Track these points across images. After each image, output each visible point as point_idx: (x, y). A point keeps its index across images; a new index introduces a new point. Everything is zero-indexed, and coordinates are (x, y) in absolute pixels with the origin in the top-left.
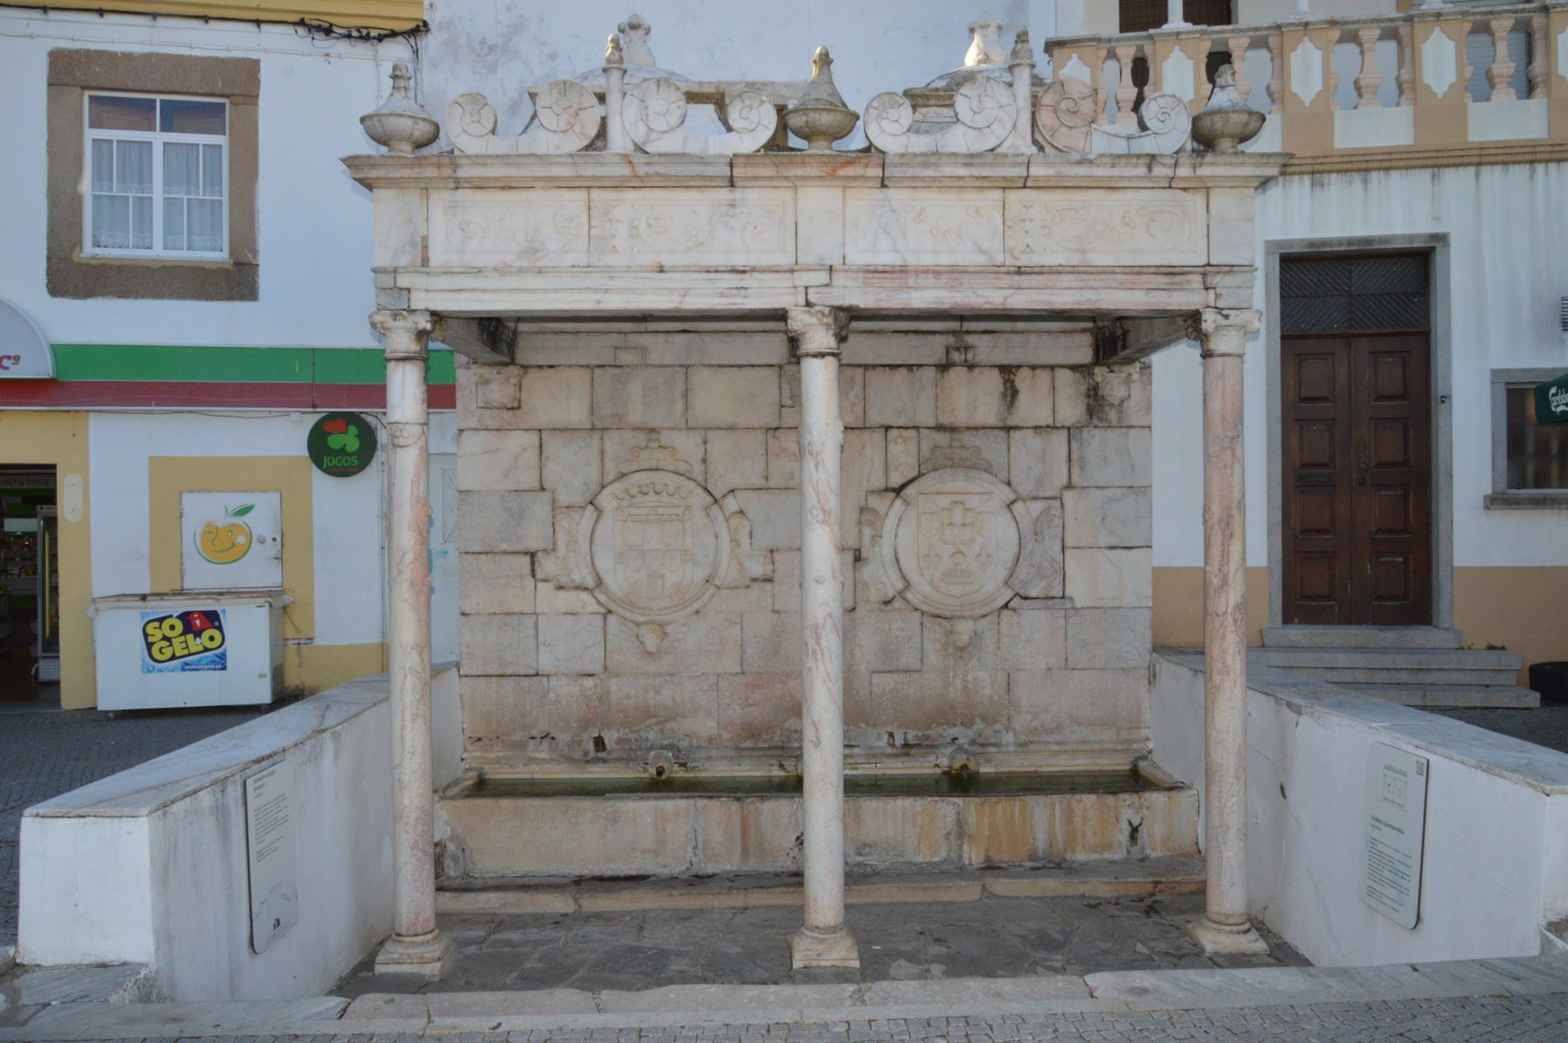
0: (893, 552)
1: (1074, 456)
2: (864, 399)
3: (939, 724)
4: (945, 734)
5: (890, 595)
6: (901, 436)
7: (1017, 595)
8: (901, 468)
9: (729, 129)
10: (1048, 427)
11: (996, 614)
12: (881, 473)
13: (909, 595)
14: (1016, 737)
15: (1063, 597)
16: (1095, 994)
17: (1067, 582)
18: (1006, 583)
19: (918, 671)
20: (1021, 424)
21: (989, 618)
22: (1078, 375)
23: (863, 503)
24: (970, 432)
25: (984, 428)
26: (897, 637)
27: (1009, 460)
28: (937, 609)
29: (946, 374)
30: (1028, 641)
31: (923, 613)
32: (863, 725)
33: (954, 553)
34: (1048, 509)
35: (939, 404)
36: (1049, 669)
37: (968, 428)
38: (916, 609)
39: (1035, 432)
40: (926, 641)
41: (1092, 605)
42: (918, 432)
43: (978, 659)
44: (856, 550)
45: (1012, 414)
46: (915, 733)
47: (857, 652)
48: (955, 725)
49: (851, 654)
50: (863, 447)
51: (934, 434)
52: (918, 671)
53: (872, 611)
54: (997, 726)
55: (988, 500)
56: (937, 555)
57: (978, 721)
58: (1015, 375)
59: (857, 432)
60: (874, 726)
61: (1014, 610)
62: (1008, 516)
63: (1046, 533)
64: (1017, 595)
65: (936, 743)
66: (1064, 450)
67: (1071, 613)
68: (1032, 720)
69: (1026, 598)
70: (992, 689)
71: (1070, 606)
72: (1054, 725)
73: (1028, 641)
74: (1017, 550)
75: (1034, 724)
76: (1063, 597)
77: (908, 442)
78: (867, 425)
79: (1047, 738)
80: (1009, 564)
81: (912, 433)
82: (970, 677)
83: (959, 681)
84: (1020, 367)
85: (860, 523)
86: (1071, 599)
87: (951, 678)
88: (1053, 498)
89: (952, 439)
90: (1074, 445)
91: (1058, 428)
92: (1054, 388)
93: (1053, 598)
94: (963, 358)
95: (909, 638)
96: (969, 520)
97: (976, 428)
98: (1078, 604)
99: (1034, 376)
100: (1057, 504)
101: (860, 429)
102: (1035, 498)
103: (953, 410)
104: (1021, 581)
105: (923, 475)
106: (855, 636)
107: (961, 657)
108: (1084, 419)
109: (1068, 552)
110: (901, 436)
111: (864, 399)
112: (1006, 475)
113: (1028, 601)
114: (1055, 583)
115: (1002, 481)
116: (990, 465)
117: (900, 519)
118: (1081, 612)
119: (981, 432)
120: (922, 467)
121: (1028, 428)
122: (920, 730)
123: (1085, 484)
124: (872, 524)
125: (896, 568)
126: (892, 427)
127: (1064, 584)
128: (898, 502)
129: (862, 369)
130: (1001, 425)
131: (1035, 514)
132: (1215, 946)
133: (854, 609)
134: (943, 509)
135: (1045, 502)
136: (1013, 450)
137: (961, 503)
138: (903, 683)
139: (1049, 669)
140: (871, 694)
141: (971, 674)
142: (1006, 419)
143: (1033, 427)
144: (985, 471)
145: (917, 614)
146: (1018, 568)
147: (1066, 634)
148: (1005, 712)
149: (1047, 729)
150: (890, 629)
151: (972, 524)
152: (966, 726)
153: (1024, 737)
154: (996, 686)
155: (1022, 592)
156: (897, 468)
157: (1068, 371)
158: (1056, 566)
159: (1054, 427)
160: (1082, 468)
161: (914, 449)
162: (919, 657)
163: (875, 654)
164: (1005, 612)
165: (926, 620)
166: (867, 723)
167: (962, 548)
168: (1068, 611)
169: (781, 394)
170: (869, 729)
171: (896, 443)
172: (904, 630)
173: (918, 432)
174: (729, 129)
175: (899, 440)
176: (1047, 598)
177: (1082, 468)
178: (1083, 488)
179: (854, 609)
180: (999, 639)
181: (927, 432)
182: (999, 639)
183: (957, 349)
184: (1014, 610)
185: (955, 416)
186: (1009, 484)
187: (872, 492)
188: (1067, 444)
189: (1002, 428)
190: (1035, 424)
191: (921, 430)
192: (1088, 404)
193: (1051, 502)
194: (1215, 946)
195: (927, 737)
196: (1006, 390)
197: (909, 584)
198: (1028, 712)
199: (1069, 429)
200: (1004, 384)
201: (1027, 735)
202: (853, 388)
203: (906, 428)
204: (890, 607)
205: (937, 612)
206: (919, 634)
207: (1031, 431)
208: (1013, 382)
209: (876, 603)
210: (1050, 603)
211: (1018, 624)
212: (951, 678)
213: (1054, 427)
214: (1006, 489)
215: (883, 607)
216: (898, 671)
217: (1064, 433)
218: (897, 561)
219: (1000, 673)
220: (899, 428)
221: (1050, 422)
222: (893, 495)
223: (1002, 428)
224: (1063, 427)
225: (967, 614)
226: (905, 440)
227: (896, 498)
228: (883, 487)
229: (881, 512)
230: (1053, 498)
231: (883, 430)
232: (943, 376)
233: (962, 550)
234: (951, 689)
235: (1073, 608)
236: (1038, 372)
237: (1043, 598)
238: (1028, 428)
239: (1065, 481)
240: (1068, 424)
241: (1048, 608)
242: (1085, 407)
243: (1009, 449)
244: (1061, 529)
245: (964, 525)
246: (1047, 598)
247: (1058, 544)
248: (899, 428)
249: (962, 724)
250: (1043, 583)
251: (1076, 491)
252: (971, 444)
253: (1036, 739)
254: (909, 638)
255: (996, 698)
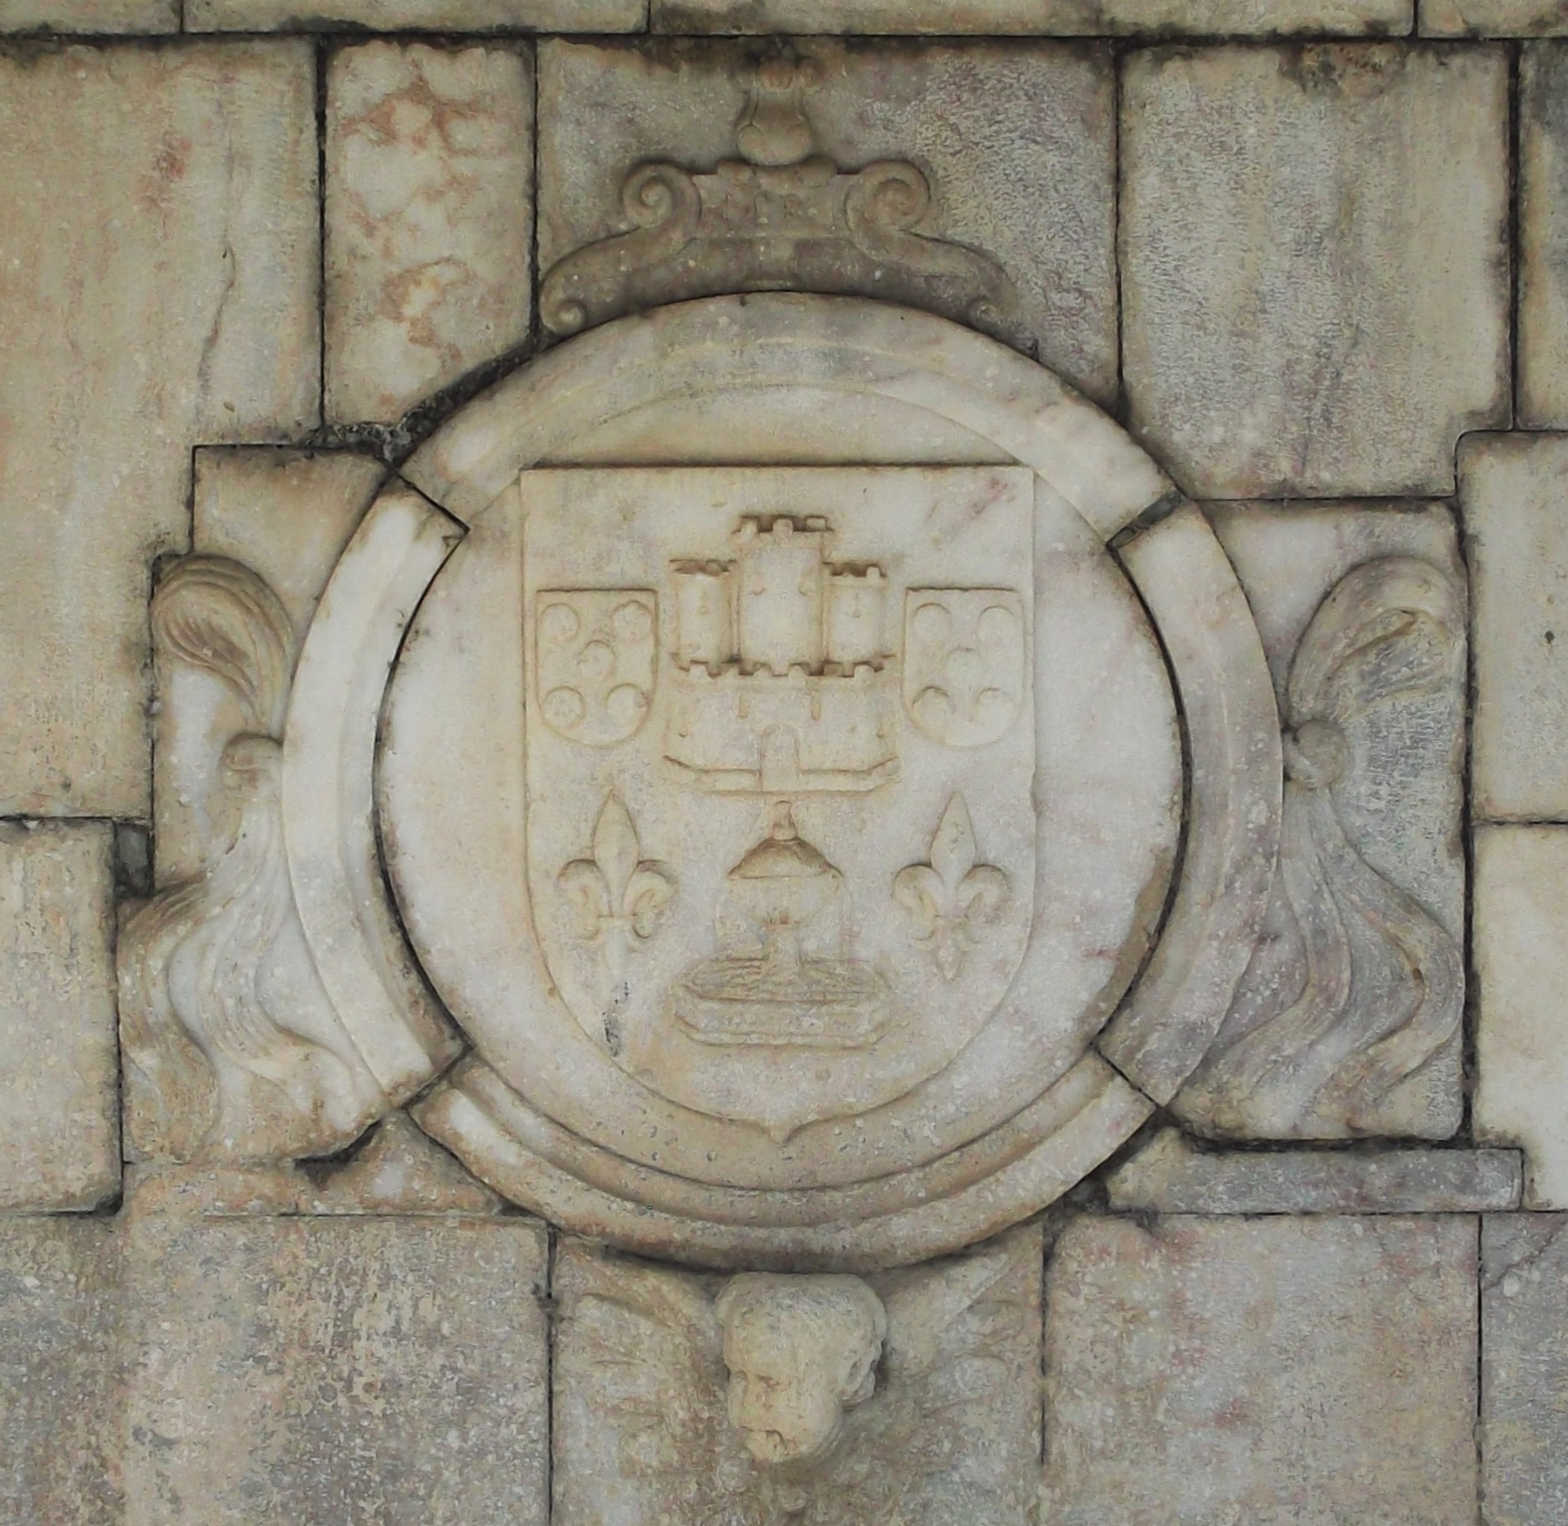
0: (362, 840)
5: (346, 1116)
6: (419, 91)
7: (1161, 1120)
8: (417, 301)
9: (793, 665)
10: (1376, 34)
11: (1030, 1245)
15: (1464, 1138)
18: (1094, 1044)
21: (978, 1274)
23: (170, 519)
24: (870, 68)
25: (958, 42)
26: (389, 1387)
28: (643, 1203)
30: (1232, 1417)
31: (554, 1235)
33: (767, 846)
38: (513, 1210)
39: (1293, 72)
40: (573, 1409)
42: (531, 67)
44: (121, 826)
49: (98, 1491)
50: (172, 164)
53: (234, 1216)
56: (646, 865)
59: (131, 63)
63: (1355, 723)
64: (1161, 1120)
71: (1504, 1196)
73: (1232, 1417)
74: (1166, 835)
76: (1464, 1138)
77: (462, 132)
86: (1515, 1150)
88: (1412, 500)
91: (1445, 47)
93: (1408, 1142)
95: (470, 1392)
101: (154, 42)
104: (1190, 1032)
105: (563, 338)
106: (121, 1375)
109: (1495, 851)
110: (419, 91)
112: (1099, 346)
114: (1408, 1050)
117: (409, 630)
119: (942, 63)
120: (556, 293)
121: (1245, 42)
125: (390, 945)
126: (359, 34)
127: (1470, 1058)
132: (82, 956)
133: (112, 1205)
134: (691, 566)
135: (1351, 524)
136: (1146, 185)
137: (800, 526)
143: (1275, 40)
144: (965, 320)
145: (523, 1241)
146: (1173, 950)
147: (1480, 1373)
150: (343, 1340)
155: (1196, 1105)
156: (392, 296)
158: (1419, 937)
163: (252, 1490)
164: (1092, 1232)
167: (813, 824)
171: (388, 135)
172: (432, 1337)
173: (531, 67)
174: (793, 665)
175: (410, 117)
176: (1358, 1144)
179: (112, 1205)
180: (1044, 1404)
181: (585, 65)
182: (1044, 1404)
184: (1146, 1218)
189: (1076, 46)
193: (1394, 528)
199: (1513, 49)
204: (342, 1196)
206: (532, 1365)
207: (1264, 64)
209: (258, 1164)
210: (1378, 1173)
211: (1176, 1305)
213: (1417, 41)
215: (300, 1191)
218: (393, 900)
220: (405, 36)
222: (366, 470)
223: (1076, 46)
224: (1471, 41)
225: (840, 1239)
226: (443, 113)
227: (382, 488)
228: (296, 413)
229: (285, 585)
230: (1412, 500)
231: (300, 56)
235: (1525, 1208)
237: (1339, 1146)
238: (1245, 42)
241: (1370, 1210)
243: (1118, 178)
244: (1453, 698)
246: (1358, 1144)
248: (405, 36)
250: (1331, 1052)
252: (873, 143)
254: (470, 1392)
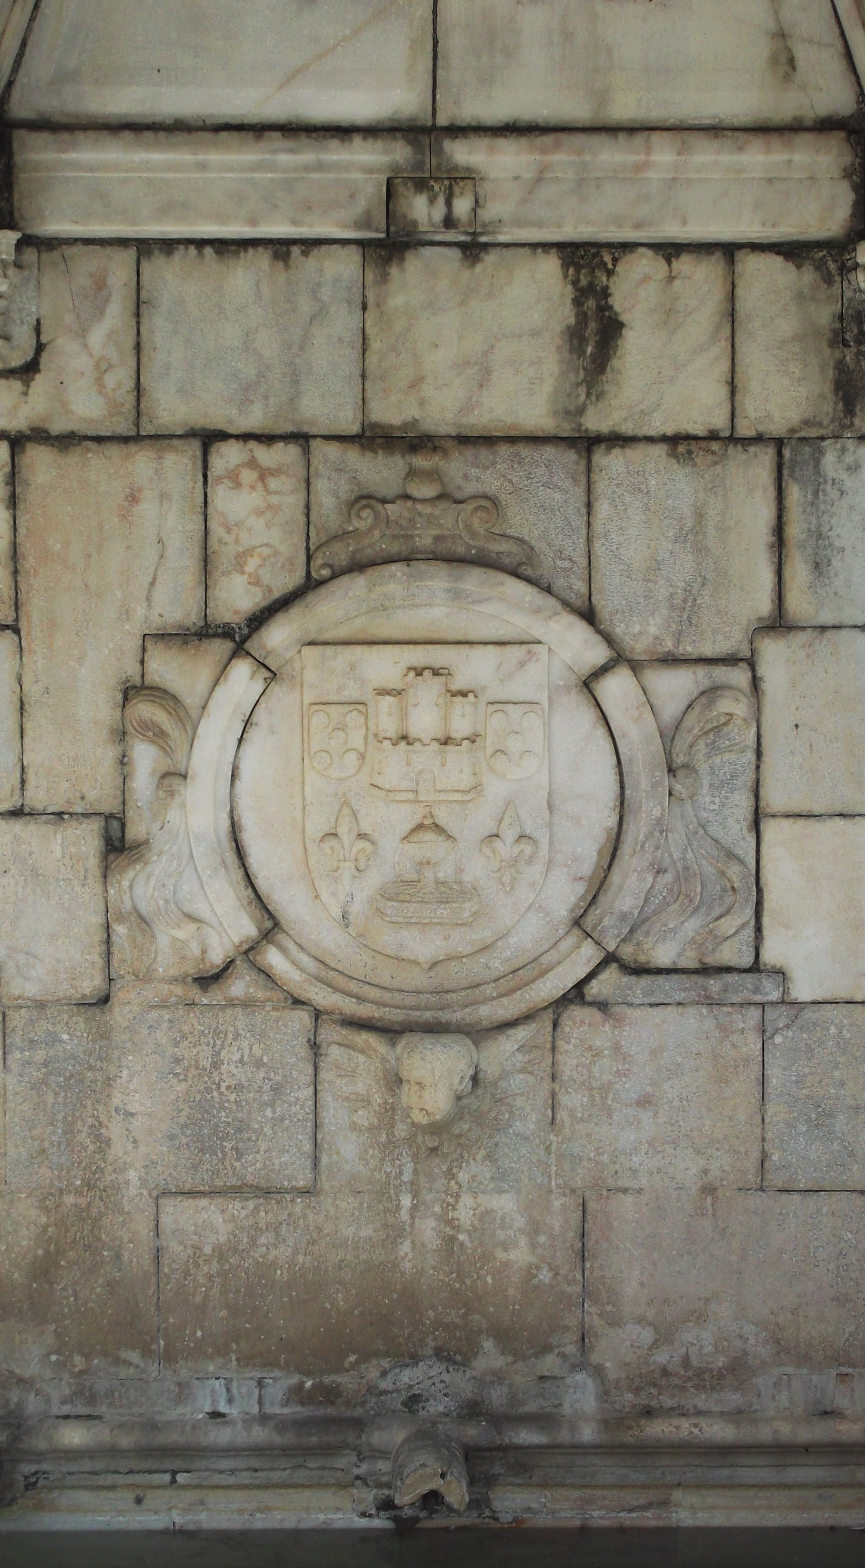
0: (225, 824)
1: (794, 530)
2: (138, 347)
3: (366, 1356)
4: (385, 1384)
5: (217, 957)
6: (252, 464)
7: (610, 959)
8: (251, 565)
10: (713, 436)
11: (547, 1018)
12: (190, 576)
13: (273, 958)
14: (604, 1395)
15: (755, 968)
16: (403, 745)
17: (766, 921)
18: (577, 922)
19: (305, 1192)
20: (628, 429)
21: (521, 1033)
22: (808, 276)
23: (132, 669)
24: (469, 452)
25: (512, 440)
26: (238, 1088)
27: (589, 540)
28: (361, 999)
29: (394, 271)
30: (644, 1102)
31: (318, 1014)
32: (134, 1356)
33: (420, 827)
34: (711, 693)
35: (372, 359)
36: (709, 1190)
37: (464, 440)
38: (297, 1002)
40: (326, 1098)
41: (845, 995)
42: (307, 452)
43: (489, 1157)
44: (109, 817)
45: (600, 396)
46: (295, 1379)
47: (115, 1130)
48: (415, 1359)
49: (98, 1137)
50: (133, 498)
51: (353, 456)
52: (305, 1192)
53: (163, 1005)
54: (549, 1363)
55: (522, 665)
56: (361, 836)
57: (488, 1345)
58: (610, 273)
59: (114, 450)
60: (169, 1357)
61: (602, 1006)
62: (587, 716)
63: (703, 768)
65: (359, 1412)
66: (766, 513)
67: (778, 1017)
68: (655, 1345)
69: (640, 970)
70: (533, 1246)
71: (775, 996)
72: (721, 1361)
74: (612, 821)
75: (662, 1358)
76: (755, 968)
77: (273, 483)
78: (148, 429)
79: (701, 1401)
80: (588, 866)
81: (288, 453)
82: (464, 1213)
83: (431, 1223)
84: (628, 247)
85: (121, 735)
86: (780, 974)
87: (404, 1215)
88: (730, 660)
89: (412, 473)
90: (795, 494)
92: (732, 315)
93: (729, 970)
94: (439, 212)
95: (277, 1090)
96: (461, 727)
97: (488, 441)
98: (802, 991)
99: (671, 279)
100: (740, 677)
101: (125, 440)
102: (671, 661)
103: (415, 384)
104: (624, 917)
105: (322, 582)
106: (109, 1082)
107: (434, 1150)
108: (829, 408)
109: (771, 830)
110: (252, 464)
111: (138, 347)
112: (580, 586)
113: (645, 981)
114: (729, 925)
115: (567, 605)
116: (530, 553)
117: (248, 723)
118: (809, 1014)
119: (504, 450)
120: (318, 561)
122: (309, 1374)
123: (827, 617)
124: (158, 736)
126: (223, 436)
128: (242, 669)
129: (132, 253)
130: (566, 429)
131: (670, 710)
132: (90, 880)
134: (383, 692)
136: (603, 509)
137: (436, 673)
138: (256, 1227)
139: (709, 1190)
140: (157, 1259)
141: (466, 1200)
142: (581, 411)
143: (664, 439)
145: (303, 1017)
146: (616, 877)
147: (763, 1081)
148: (571, 1320)
149: (700, 1373)
150: (216, 1065)
151: (472, 739)
152: (449, 1360)
153: (629, 1396)
154: (542, 1239)
155: (627, 952)
157: (779, 260)
159: (733, 439)
160: (818, 567)
161: (292, 502)
162: (308, 1147)
163: (172, 1137)
164: (576, 1014)
165: (330, 1033)
166: (147, 1352)
167: (443, 817)
168: (770, 1014)
169: (15, 529)
170: (153, 1368)
171: (238, 485)
173: (307, 452)
175: (248, 476)
176: (705, 970)
177: (818, 567)
178: (823, 628)
179: (105, 1000)
180: (553, 1095)
181: (333, 450)
182: (553, 1095)
183: (421, 185)
184: (602, 1006)
185: (422, 403)
186: (589, 615)
187: (163, 637)
188: (772, 493)
190: (669, 430)
191: (316, 445)
192: (840, 366)
193: (722, 674)
194: (90, 880)
195: (330, 1394)
196: (582, 318)
197: (276, 924)
198: (641, 1321)
199: (779, 443)
200: (577, 302)
201: (637, 1391)
202: (102, 313)
203: (267, 439)
204: (215, 996)
205: (364, 1011)
207: (659, 451)
208: (605, 293)
209: (175, 980)
210: (714, 985)
212: (404, 1215)
213: (733, 439)
214: (581, 630)
215: (195, 993)
216: (237, 1191)
217: (766, 457)
219: (557, 1204)
220: (246, 437)
221: (719, 421)
222: (228, 646)
224: (759, 439)
226: (264, 474)
228: (192, 617)
229: (188, 701)
230: (730, 660)
232: (384, 277)
233: (442, 820)
234: (406, 1247)
235: (785, 1001)
236: (684, 264)
239: (764, 606)
240: (777, 427)
241: (710, 1002)
242: (830, 373)
243: (589, 505)
244: (751, 756)
245: (446, 741)
246: (705, 970)
247: (742, 802)
248: (246, 437)
249: (439, 1353)
250: (692, 926)
251: (802, 637)
252: (471, 488)
253: (668, 1402)
254: (277, 1090)
255: (545, 1276)
